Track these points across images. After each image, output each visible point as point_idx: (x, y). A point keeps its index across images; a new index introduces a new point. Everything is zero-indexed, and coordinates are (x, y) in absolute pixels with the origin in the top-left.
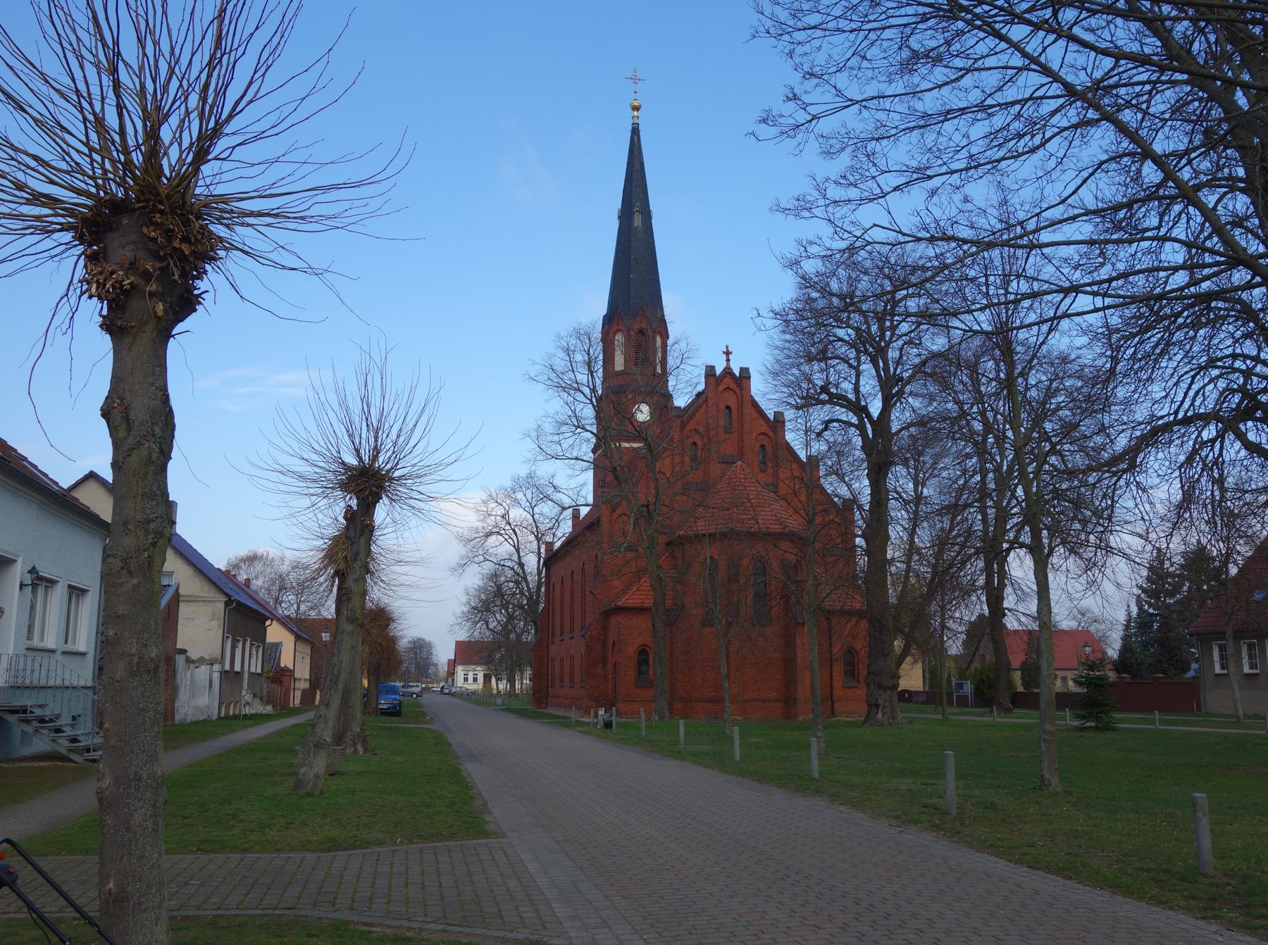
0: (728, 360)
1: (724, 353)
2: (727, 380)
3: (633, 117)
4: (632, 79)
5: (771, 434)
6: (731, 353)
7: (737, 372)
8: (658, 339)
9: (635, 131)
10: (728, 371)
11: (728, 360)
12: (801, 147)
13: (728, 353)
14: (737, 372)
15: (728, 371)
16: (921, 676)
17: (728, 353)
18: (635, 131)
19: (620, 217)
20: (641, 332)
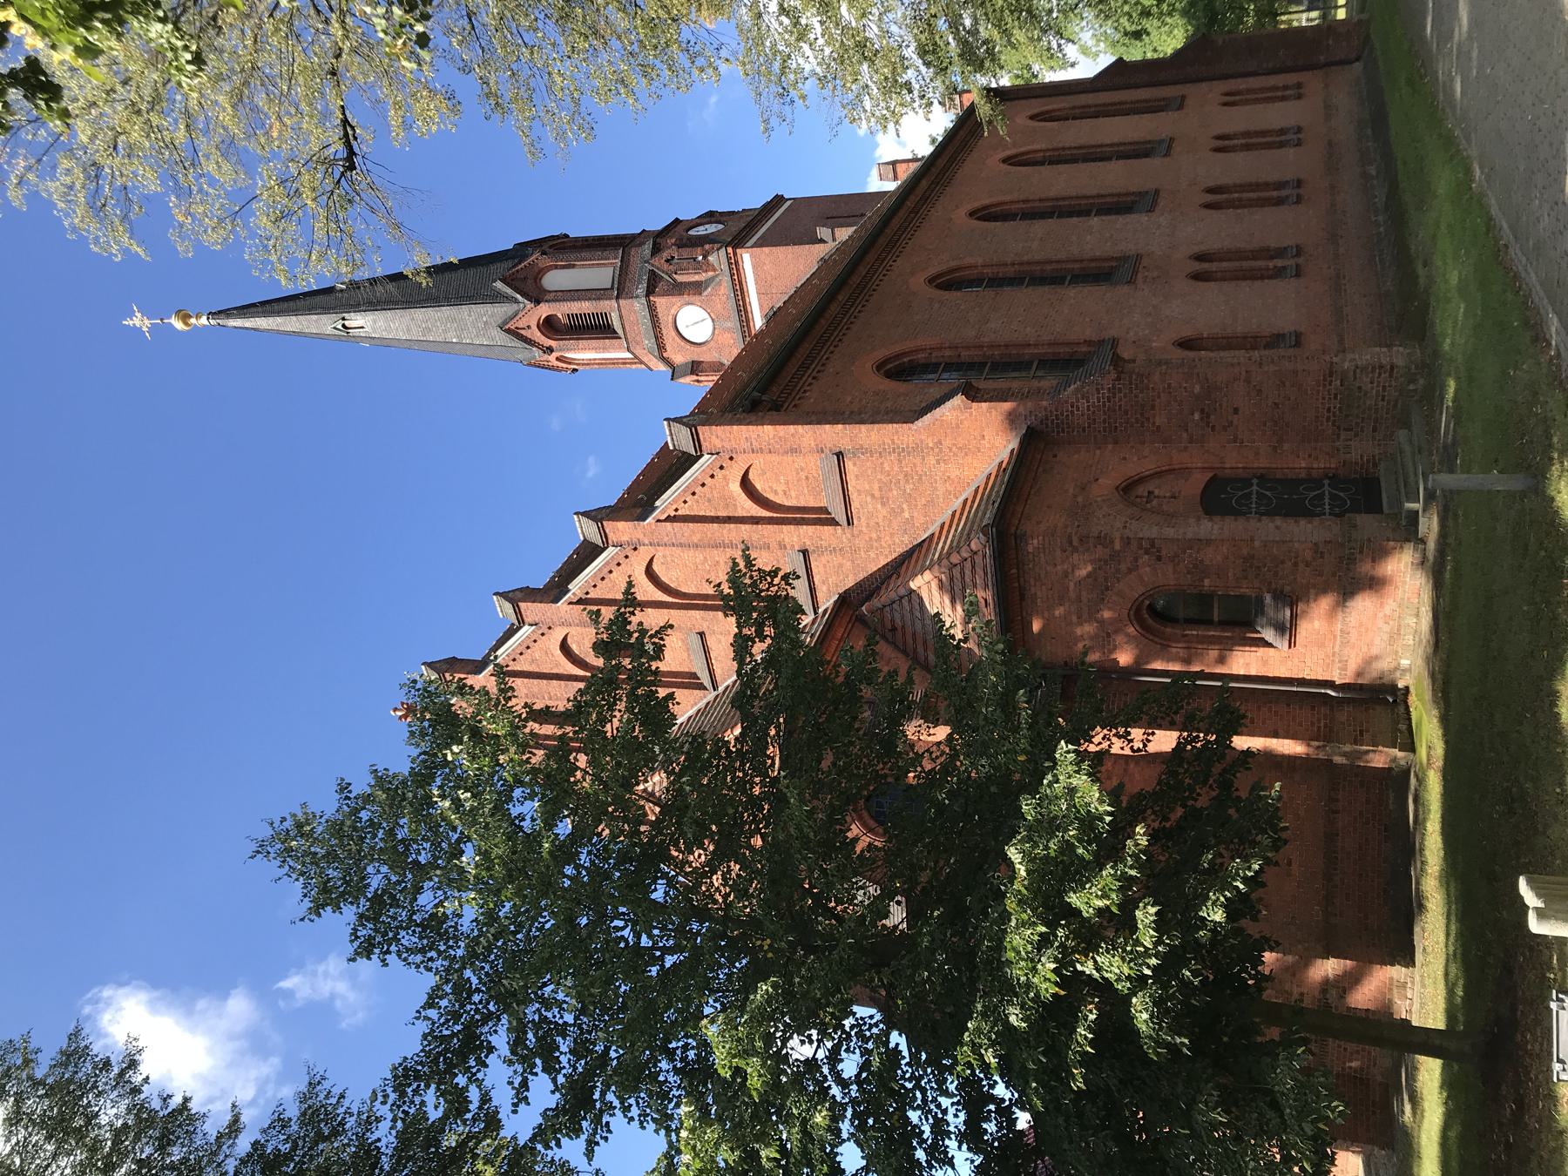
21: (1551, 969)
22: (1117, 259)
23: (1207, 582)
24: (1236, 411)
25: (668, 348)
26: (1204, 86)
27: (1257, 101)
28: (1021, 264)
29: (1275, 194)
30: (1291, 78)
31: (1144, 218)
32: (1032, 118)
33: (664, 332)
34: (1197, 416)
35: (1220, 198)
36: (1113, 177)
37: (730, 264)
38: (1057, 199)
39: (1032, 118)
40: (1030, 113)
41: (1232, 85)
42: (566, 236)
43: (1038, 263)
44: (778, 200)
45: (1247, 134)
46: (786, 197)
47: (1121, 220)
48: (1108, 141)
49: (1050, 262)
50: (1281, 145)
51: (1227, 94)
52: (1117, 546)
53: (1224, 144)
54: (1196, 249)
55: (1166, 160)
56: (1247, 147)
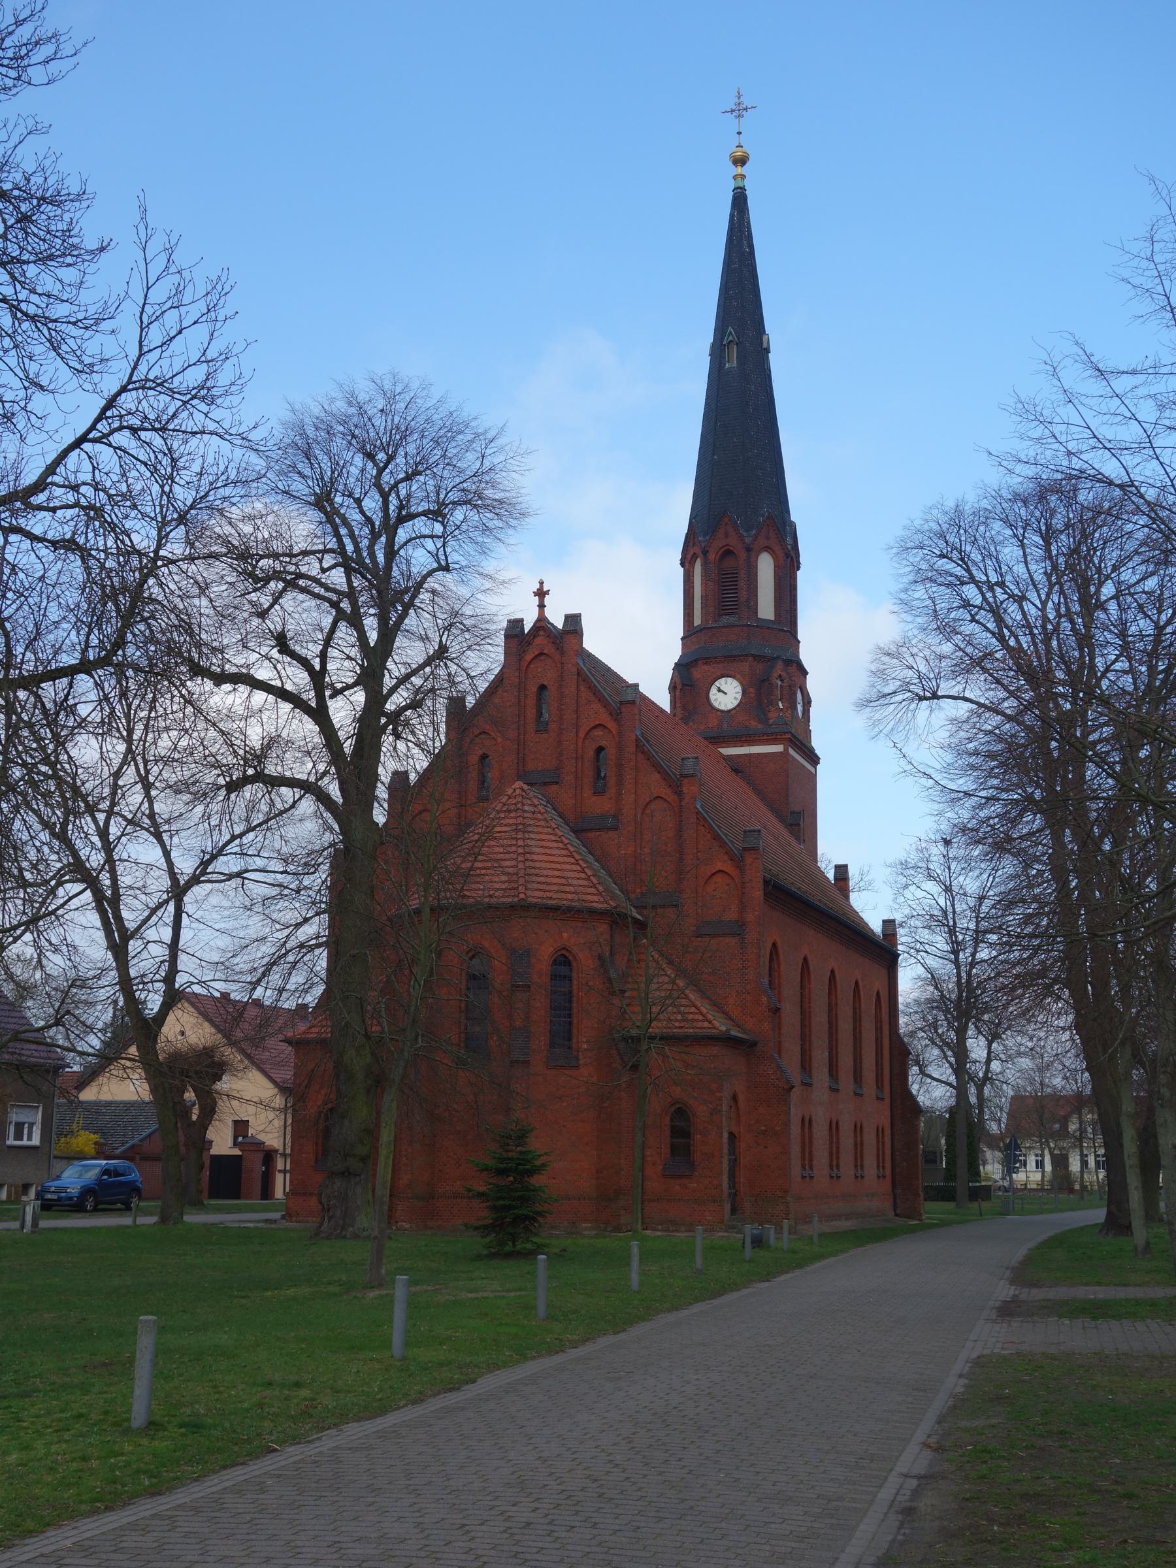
0: (542, 606)
1: (536, 594)
2: (539, 640)
3: (735, 178)
4: (746, 109)
5: (612, 725)
6: (547, 592)
7: (559, 624)
8: (766, 566)
9: (740, 201)
10: (542, 624)
11: (542, 606)
12: (142, 209)
13: (541, 594)
14: (559, 624)
15: (542, 624)
16: (873, 1038)
17: (541, 594)
18: (740, 201)
19: (711, 354)
20: (728, 553)
21: (1093, 1123)
22: (810, 1071)
23: (699, 1136)
24: (766, 1147)
25: (706, 667)
26: (888, 1113)
27: (878, 1150)
28: (810, 1012)
29: (834, 1163)
30: (888, 1172)
31: (827, 1085)
32: (878, 993)
33: (721, 666)
34: (763, 1128)
35: (834, 1128)
36: (846, 1060)
37: (776, 734)
38: (837, 1026)
39: (878, 993)
40: (881, 992)
41: (888, 1132)
42: (798, 568)
43: (810, 1022)
44: (814, 760)
45: (862, 1144)
46: (818, 767)
47: (826, 1070)
48: (863, 1052)
49: (810, 1031)
50: (856, 1166)
51: (861, 1126)
52: (717, 1094)
53: (858, 1129)
54: (813, 1118)
55: (852, 1094)
56: (856, 1145)
